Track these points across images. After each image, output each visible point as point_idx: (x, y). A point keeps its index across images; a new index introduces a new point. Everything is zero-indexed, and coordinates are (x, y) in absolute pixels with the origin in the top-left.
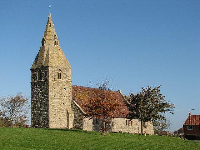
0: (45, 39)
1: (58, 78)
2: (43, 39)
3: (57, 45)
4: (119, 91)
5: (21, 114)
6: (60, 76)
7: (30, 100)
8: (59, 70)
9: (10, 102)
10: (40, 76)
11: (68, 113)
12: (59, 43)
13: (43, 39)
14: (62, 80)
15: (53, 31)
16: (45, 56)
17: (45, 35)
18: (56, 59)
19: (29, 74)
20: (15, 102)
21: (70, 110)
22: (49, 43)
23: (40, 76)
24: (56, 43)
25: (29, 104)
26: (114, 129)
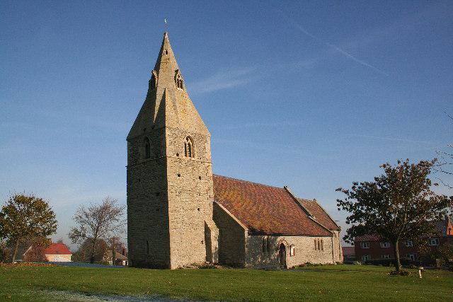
0: (155, 74)
1: (186, 156)
2: (153, 76)
3: (182, 87)
4: (286, 189)
5: (112, 234)
6: (189, 151)
7: (125, 211)
8: (187, 139)
9: (94, 215)
10: (147, 148)
11: (206, 225)
12: (184, 85)
13: (153, 76)
14: (193, 159)
15: (172, 62)
16: (157, 108)
17: (157, 68)
18: (182, 117)
19: (125, 145)
20: (103, 214)
21: (212, 224)
22: (165, 83)
23: (147, 148)
24: (180, 84)
25: (124, 217)
26: (291, 262)
